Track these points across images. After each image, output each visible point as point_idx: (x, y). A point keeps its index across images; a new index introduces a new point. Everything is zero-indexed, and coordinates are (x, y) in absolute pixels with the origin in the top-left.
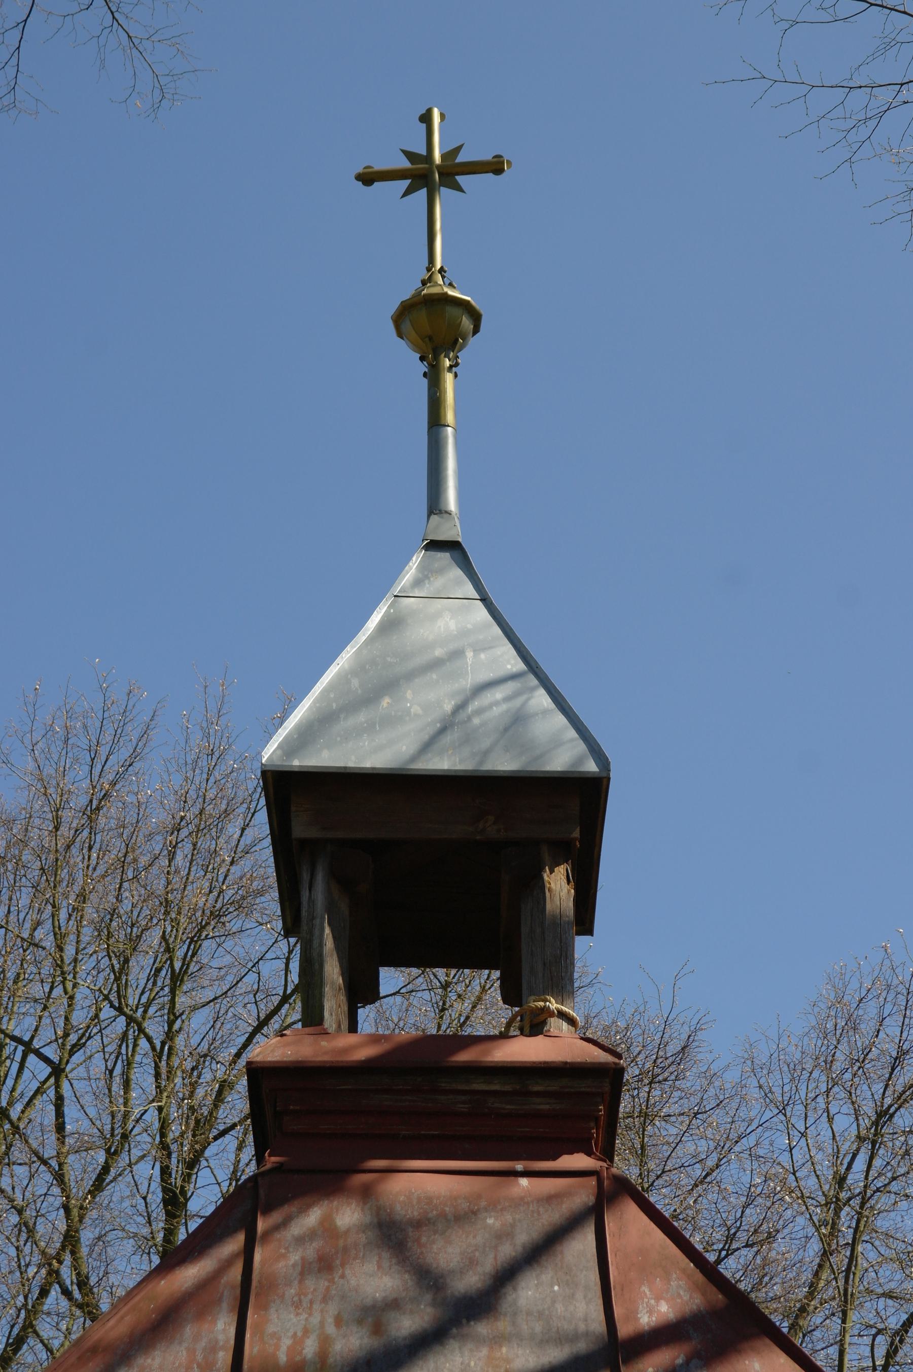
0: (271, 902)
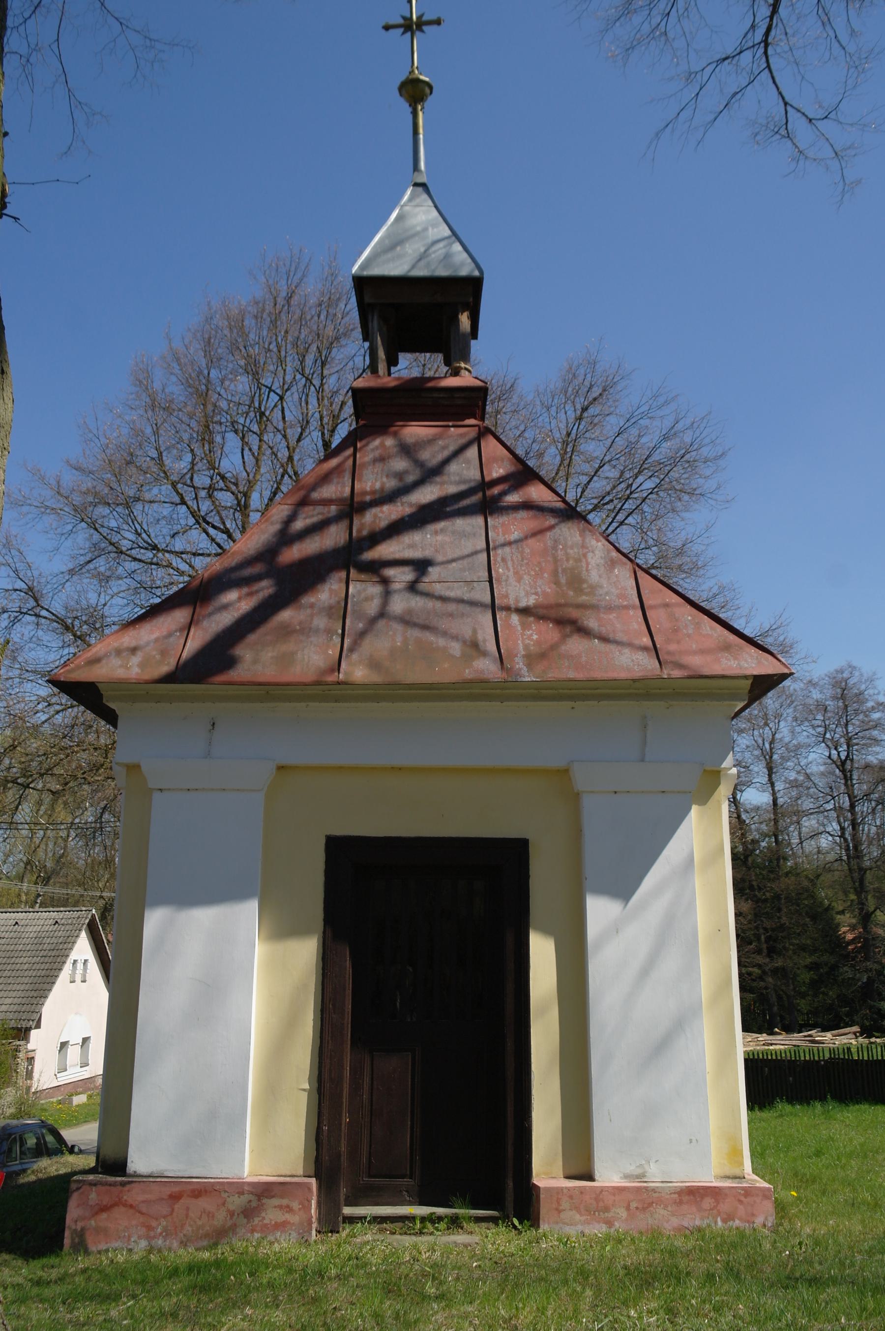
0: (358, 333)
